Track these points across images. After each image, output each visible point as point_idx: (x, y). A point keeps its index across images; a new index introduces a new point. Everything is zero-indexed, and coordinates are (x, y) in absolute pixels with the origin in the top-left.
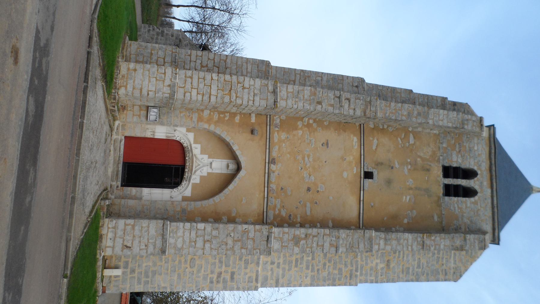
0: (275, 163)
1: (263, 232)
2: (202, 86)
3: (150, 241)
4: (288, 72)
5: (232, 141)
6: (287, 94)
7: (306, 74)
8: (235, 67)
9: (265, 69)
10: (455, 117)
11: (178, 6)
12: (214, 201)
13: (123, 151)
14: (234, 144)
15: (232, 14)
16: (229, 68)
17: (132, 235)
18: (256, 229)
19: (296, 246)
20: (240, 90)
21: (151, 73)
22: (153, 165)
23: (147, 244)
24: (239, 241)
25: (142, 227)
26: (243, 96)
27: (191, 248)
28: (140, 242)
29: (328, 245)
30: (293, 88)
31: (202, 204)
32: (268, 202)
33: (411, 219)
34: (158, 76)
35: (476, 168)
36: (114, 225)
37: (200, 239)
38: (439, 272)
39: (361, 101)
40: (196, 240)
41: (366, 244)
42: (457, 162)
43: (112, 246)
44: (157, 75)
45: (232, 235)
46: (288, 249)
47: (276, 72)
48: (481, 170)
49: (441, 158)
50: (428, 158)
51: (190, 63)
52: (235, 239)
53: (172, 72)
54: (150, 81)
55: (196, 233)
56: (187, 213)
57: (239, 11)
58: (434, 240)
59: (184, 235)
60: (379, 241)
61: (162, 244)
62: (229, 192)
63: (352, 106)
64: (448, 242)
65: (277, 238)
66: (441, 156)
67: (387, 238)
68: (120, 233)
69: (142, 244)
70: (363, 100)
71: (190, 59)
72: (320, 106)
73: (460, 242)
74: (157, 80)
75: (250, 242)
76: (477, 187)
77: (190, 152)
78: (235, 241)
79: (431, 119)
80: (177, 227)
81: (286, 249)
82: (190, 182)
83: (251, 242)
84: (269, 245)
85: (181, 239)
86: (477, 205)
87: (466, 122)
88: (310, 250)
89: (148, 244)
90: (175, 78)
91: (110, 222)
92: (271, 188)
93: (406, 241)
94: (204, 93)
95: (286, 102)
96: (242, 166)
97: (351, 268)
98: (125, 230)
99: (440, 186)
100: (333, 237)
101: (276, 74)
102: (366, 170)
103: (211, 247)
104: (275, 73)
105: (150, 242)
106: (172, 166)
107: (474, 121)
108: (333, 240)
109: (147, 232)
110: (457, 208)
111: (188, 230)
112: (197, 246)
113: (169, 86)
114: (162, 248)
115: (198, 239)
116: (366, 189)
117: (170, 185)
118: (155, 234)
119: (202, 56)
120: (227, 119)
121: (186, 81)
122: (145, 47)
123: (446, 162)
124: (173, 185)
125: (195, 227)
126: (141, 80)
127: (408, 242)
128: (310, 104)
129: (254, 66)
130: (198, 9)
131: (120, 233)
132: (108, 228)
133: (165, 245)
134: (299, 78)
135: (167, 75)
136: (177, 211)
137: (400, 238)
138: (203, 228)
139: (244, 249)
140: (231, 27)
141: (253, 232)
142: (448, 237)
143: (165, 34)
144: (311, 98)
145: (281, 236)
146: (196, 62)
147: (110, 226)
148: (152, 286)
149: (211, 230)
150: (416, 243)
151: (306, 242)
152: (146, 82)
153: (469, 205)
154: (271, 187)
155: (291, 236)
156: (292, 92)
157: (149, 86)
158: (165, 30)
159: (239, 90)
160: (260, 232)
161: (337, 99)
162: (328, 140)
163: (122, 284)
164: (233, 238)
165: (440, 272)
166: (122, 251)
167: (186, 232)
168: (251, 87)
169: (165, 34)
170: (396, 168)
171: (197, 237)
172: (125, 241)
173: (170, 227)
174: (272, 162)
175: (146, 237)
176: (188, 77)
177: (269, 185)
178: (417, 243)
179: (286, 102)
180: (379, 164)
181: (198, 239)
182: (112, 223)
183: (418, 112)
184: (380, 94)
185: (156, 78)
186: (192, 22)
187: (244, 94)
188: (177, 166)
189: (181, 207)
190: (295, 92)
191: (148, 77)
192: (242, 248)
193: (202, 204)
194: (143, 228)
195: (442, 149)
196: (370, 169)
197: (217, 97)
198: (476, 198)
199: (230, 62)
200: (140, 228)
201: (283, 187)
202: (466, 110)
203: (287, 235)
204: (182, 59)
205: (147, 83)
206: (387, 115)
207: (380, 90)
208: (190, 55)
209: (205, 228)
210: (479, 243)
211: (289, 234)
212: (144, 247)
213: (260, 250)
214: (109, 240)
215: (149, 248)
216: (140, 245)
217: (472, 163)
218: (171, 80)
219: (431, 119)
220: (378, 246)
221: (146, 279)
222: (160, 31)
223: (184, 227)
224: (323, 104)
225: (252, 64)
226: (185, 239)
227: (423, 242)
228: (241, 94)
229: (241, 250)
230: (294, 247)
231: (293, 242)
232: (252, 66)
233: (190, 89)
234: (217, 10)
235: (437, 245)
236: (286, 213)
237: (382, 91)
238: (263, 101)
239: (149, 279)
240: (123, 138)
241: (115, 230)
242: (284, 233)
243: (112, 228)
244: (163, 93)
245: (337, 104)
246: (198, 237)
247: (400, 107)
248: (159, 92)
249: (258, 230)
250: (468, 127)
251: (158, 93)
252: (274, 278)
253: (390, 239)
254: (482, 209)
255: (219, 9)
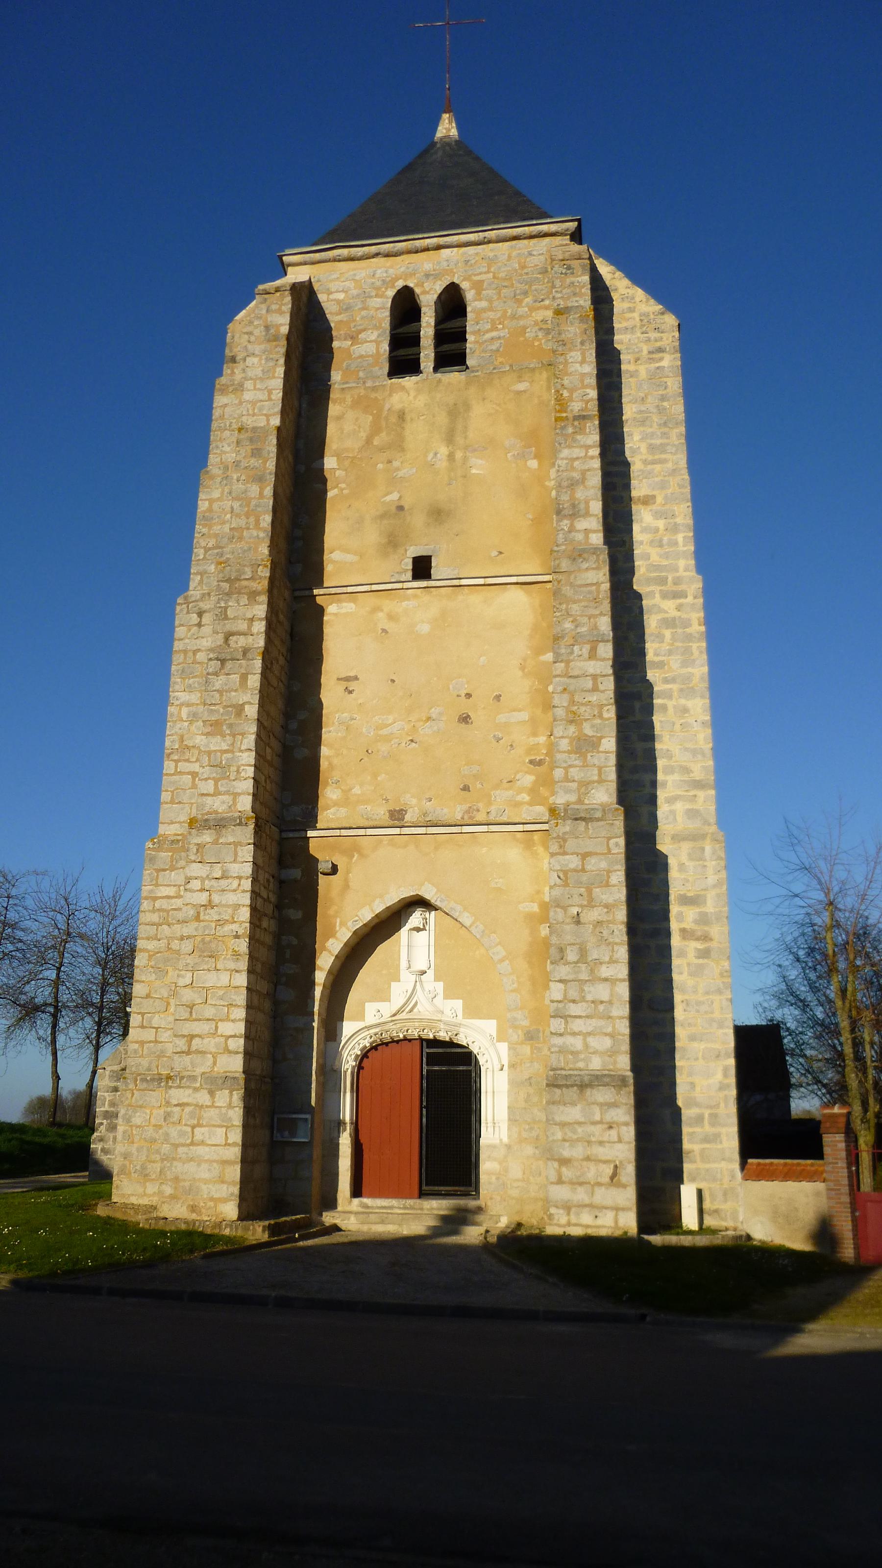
0: (402, 810)
1: (564, 833)
2: (209, 1012)
3: (597, 1117)
4: (172, 792)
5: (350, 924)
6: (220, 794)
7: (177, 747)
8: (165, 927)
9: (167, 851)
10: (261, 360)
11: (57, 1078)
12: (501, 961)
13: (390, 1200)
14: (357, 918)
15: (69, 934)
16: (169, 944)
17: (585, 1163)
18: (558, 851)
19: (599, 745)
20: (213, 914)
21: (182, 1141)
22: (424, 1120)
23: (606, 1126)
24: (590, 891)
25: (564, 1140)
26: (228, 906)
27: (611, 1012)
28: (601, 1143)
29: (592, 663)
30: (206, 779)
31: (512, 991)
32: (501, 822)
33: (528, 450)
34: (189, 1123)
35: (391, 293)
36: (561, 1211)
37: (590, 992)
38: (658, 368)
39: (230, 604)
40: (593, 1002)
41: (239, 743)
42: (377, 343)
43: (614, 1212)
44: (185, 1125)
45: (574, 910)
46: (606, 767)
47: (176, 823)
48: (397, 279)
49: (369, 384)
50: (371, 418)
51: (161, 1042)
52: (585, 903)
53: (179, 1087)
54: (202, 1143)
55: (574, 1001)
56: (535, 1027)
57: (59, 917)
58: (571, 391)
59: (579, 1033)
60: (579, 531)
61: (605, 1086)
62: (478, 923)
63: (243, 626)
64: (573, 354)
65: (579, 796)
66: (364, 383)
67: (571, 513)
68: (581, 1195)
69: (605, 1139)
70: (226, 602)
71: (150, 1042)
72: (247, 707)
73: (572, 324)
74: (199, 1125)
75: (593, 864)
76: (439, 287)
77: (386, 1027)
78: (591, 903)
79: (268, 420)
80: (560, 1052)
81: (607, 769)
82: (460, 1024)
83: (593, 861)
84: (598, 814)
85: (590, 1039)
86: (483, 281)
87: (272, 331)
88: (606, 708)
89: (607, 1123)
90: (193, 1078)
91: (555, 1222)
92: (466, 817)
93: (576, 463)
94: (226, 1004)
95: (239, 794)
96: (412, 894)
97: (657, 595)
98: (572, 1183)
99: (440, 381)
100: (572, 653)
101: (179, 822)
102: (409, 575)
103: (609, 963)
104: (177, 826)
105: (602, 1119)
106: (425, 1073)
107: (268, 311)
108: (580, 653)
109: (576, 1126)
110: (494, 334)
111: (567, 1022)
112: (606, 998)
113: (212, 1093)
114: (614, 1086)
115: (589, 997)
116: (456, 572)
117: (473, 1075)
118: (579, 1107)
119: (143, 1014)
120: (295, 942)
121: (198, 1052)
122: (125, 1158)
123: (381, 368)
124: (472, 1068)
125: (560, 1005)
126: (199, 1165)
127: (577, 458)
128: (243, 734)
129: (160, 881)
130: (61, 1025)
131: (581, 1195)
132: (569, 1224)
133: (607, 1080)
134: (187, 764)
135: (185, 1100)
136: (532, 1053)
137: (568, 479)
138: (561, 986)
139: (609, 877)
140: (105, 933)
141: (567, 857)
142: (562, 354)
143: (112, 1109)
144: (228, 732)
145: (574, 785)
146: (157, 1028)
147: (564, 1220)
148: (722, 1105)
149: (565, 965)
150: (579, 437)
151: (586, 720)
152: (201, 1150)
153: (484, 304)
154: (463, 818)
155: (574, 760)
156: (216, 781)
157: (213, 1143)
158: (102, 1109)
159: (216, 917)
160: (565, 840)
161: (229, 665)
162: (338, 679)
163: (721, 1180)
164: (582, 906)
165: (657, 365)
166: (624, 1186)
167: (571, 1029)
168: (207, 888)
169: (112, 1109)
170: (400, 497)
171: (583, 999)
172: (599, 1180)
173: (562, 1069)
174: (399, 820)
175: (592, 1128)
176: (190, 1046)
177: (459, 823)
178: (580, 434)
179: (239, 794)
180: (392, 543)
181: (589, 997)
182: (556, 1217)
183: (252, 456)
184: (217, 553)
185: (193, 1127)
186: (98, 1036)
187: (223, 902)
188: (424, 1059)
189: (522, 1043)
190: (214, 775)
191: (191, 1147)
192: (607, 885)
193: (512, 991)
194: (567, 1137)
195: (347, 383)
196: (407, 564)
197: (237, 971)
198: (464, 285)
199: (155, 942)
200: (567, 1144)
201: (461, 786)
202: (245, 330)
203: (571, 770)
204: (150, 1063)
205: (207, 1149)
206: (262, 535)
207: (206, 552)
208: (142, 1043)
209: (560, 981)
210: (573, 273)
211: (570, 766)
212: (613, 1133)
213: (609, 839)
214: (599, 1222)
215: (615, 1119)
216: (609, 1142)
217: (376, 302)
218: (196, 1090)
219: (268, 420)
220: (590, 535)
221: (706, 1122)
222: (105, 1121)
223: (561, 1035)
224: (241, 702)
225: (157, 885)
226: (590, 1029)
227: (576, 418)
228: (226, 911)
229: (614, 886)
230: (601, 749)
231: (589, 755)
232: (161, 885)
233: (217, 1039)
234: (62, 974)
235: (582, 381)
236: (526, 772)
237: (210, 549)
238: (240, 854)
239: (707, 1113)
240: (356, 1201)
241: (575, 1206)
242: (567, 779)
243: (568, 1214)
244: (230, 1106)
245: (241, 666)
246: (584, 997)
247: (240, 502)
248: (229, 1116)
249: (561, 847)
250: (281, 325)
251: (230, 1119)
252: (692, 793)
253: (574, 506)
254: (492, 270)
255: (59, 969)
